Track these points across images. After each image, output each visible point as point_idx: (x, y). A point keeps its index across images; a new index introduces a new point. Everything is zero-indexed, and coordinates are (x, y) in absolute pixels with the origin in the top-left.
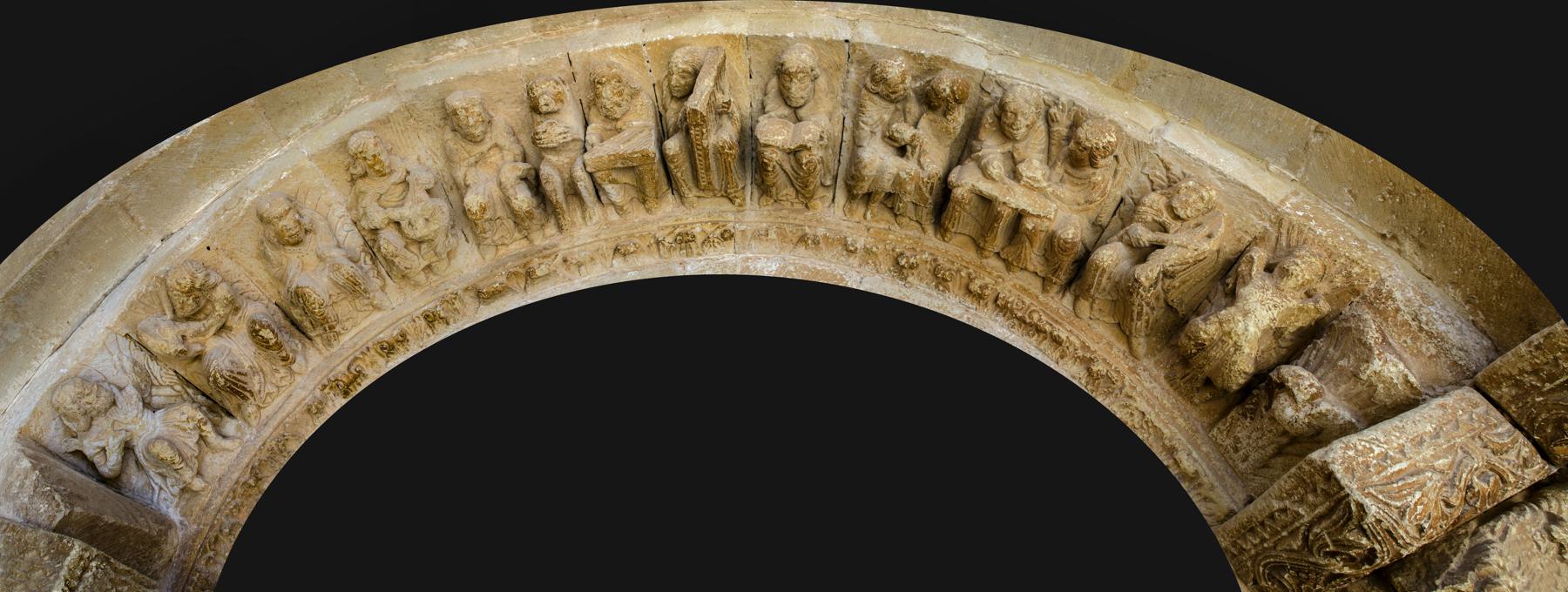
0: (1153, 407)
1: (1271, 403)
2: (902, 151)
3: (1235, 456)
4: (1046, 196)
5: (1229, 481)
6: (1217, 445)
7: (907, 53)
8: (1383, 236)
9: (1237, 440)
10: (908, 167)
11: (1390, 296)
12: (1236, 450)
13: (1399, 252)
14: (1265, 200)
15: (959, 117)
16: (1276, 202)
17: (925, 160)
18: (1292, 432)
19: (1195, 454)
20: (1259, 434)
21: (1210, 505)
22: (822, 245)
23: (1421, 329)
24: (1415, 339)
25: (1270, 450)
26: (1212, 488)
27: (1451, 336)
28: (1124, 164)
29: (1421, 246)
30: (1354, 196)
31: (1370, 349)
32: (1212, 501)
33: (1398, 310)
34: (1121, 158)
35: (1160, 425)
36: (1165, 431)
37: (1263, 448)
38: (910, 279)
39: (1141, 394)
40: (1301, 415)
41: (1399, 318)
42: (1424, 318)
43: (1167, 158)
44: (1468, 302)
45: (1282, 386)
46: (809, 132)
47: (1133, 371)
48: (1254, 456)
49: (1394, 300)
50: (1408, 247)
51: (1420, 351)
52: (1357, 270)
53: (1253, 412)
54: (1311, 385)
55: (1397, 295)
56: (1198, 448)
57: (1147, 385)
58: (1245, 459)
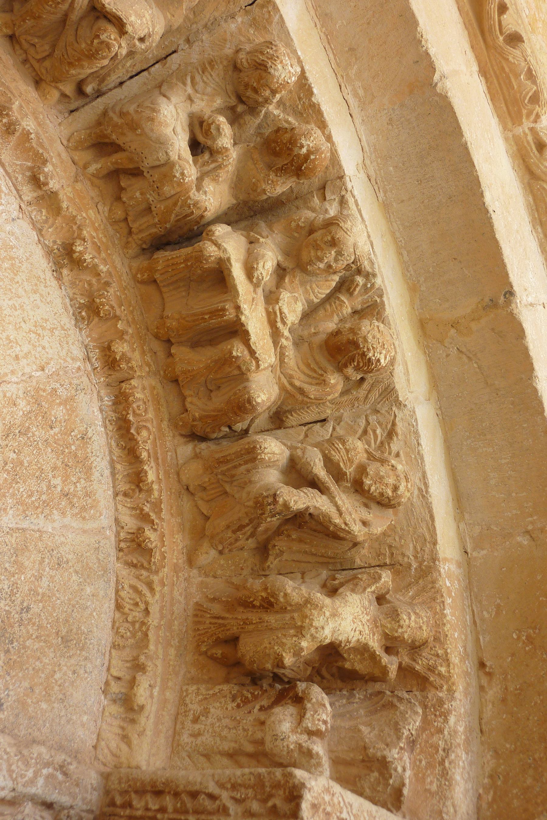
0: (162, 617)
1: (271, 707)
2: (195, 146)
3: (188, 724)
4: (276, 343)
5: (162, 740)
6: (182, 701)
7: (303, 71)
8: (482, 665)
9: (206, 712)
10: (189, 170)
11: (445, 716)
12: (196, 720)
13: (482, 688)
14: (435, 543)
15: (280, 187)
16: (441, 555)
17: (209, 186)
18: (268, 745)
19: (156, 691)
20: (231, 724)
21: (124, 747)
22: (13, 139)
23: (442, 763)
24: (430, 765)
25: (226, 746)
26: (141, 734)
27: (457, 789)
28: (362, 393)
29: (504, 700)
30: (498, 613)
31: (399, 738)
32: (129, 744)
33: (440, 731)
34: (366, 386)
35: (151, 634)
36: (152, 647)
37: (223, 739)
38: (65, 272)
39: (163, 596)
40: (293, 738)
41: (435, 739)
42: (453, 756)
43: (400, 427)
44: (491, 777)
45: (299, 701)
46: (140, 16)
47: (176, 569)
48: (207, 739)
49: (446, 721)
50: (493, 692)
51: (424, 779)
52: (443, 670)
53: (246, 701)
54: (325, 722)
55: (452, 719)
56: (163, 690)
57: (176, 594)
58: (196, 735)
